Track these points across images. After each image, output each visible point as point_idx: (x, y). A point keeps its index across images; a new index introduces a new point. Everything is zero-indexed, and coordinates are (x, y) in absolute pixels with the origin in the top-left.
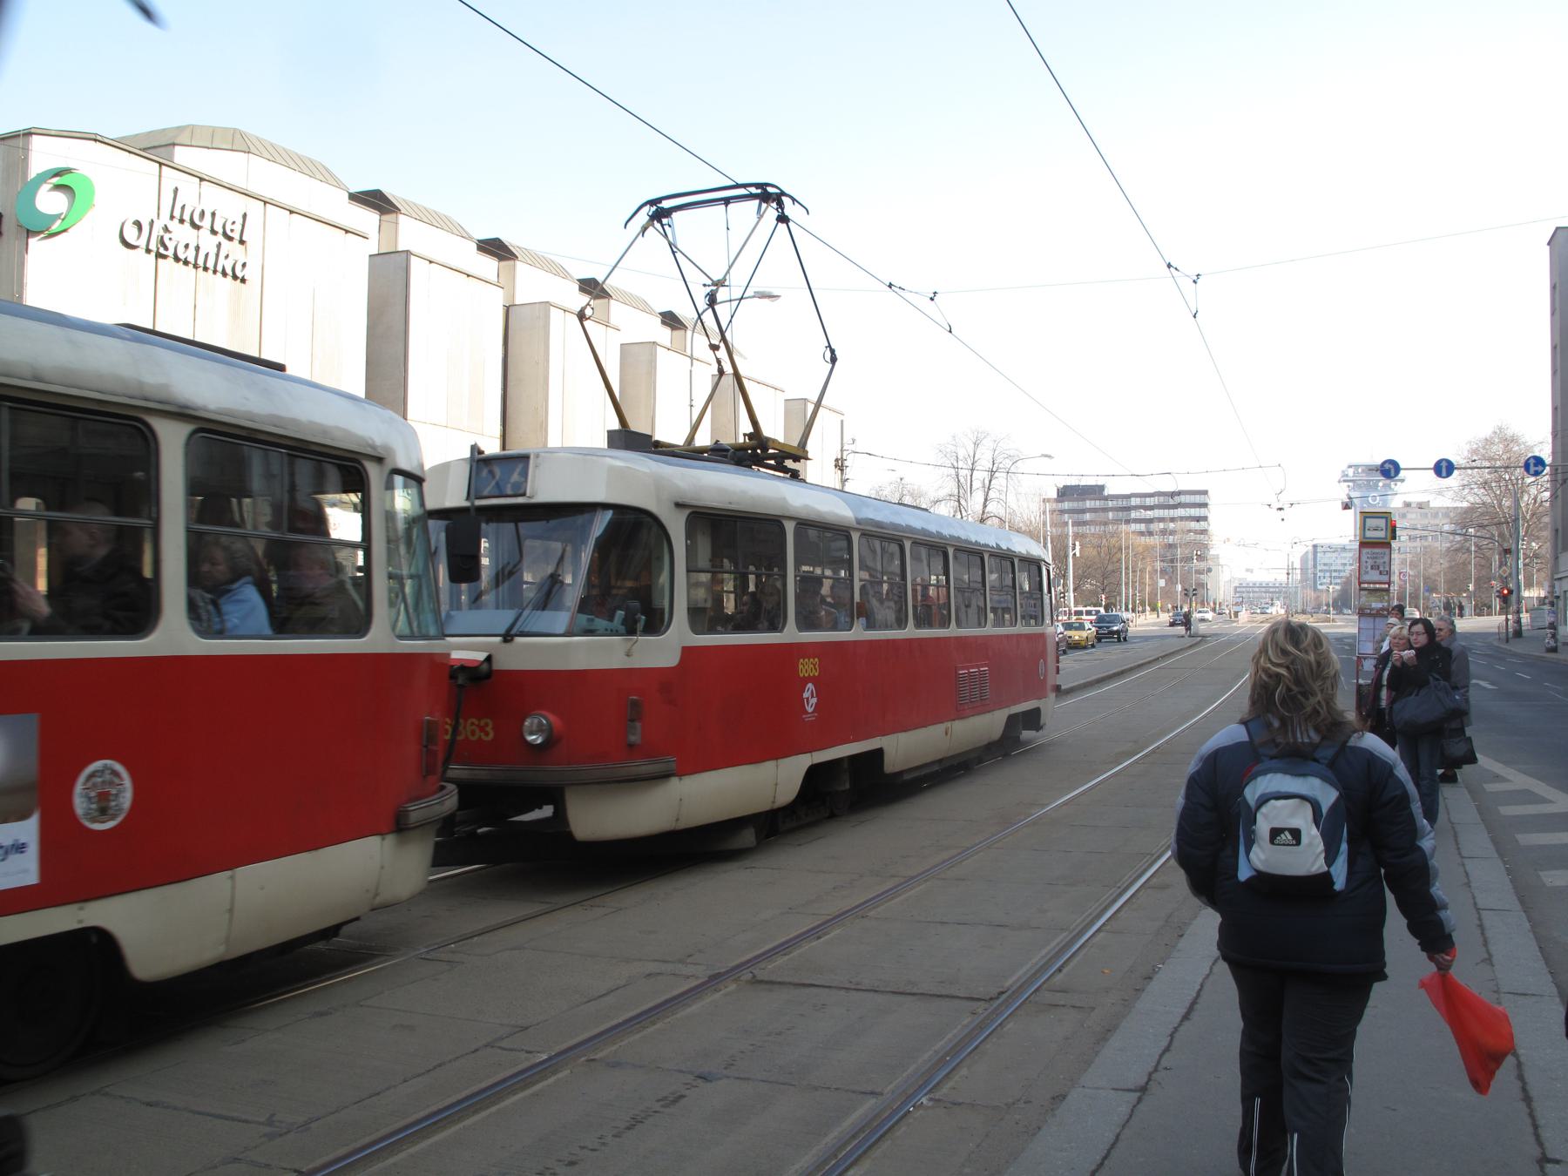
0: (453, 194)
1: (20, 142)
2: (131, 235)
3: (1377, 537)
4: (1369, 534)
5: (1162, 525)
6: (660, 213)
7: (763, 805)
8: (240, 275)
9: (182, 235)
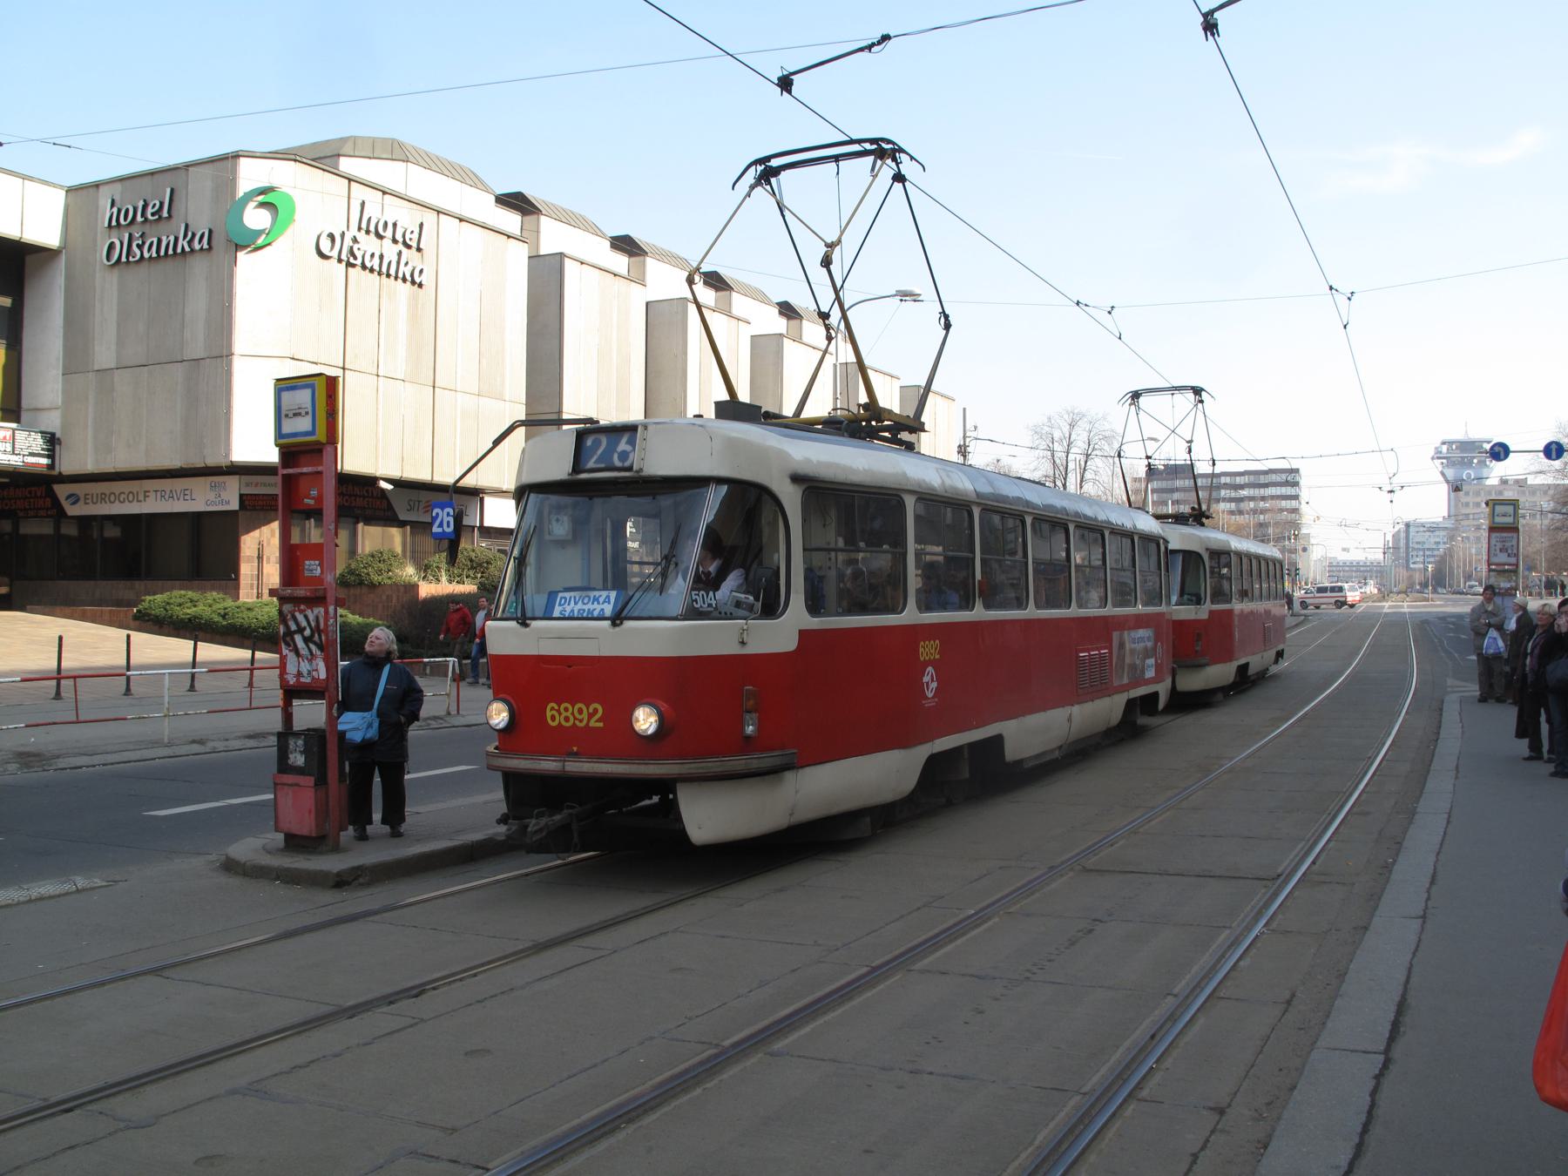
0: (590, 193)
1: (229, 163)
2: (325, 246)
3: (1504, 522)
4: (1497, 519)
5: (1252, 504)
6: (767, 172)
7: (887, 796)
8: (417, 280)
9: (368, 244)
